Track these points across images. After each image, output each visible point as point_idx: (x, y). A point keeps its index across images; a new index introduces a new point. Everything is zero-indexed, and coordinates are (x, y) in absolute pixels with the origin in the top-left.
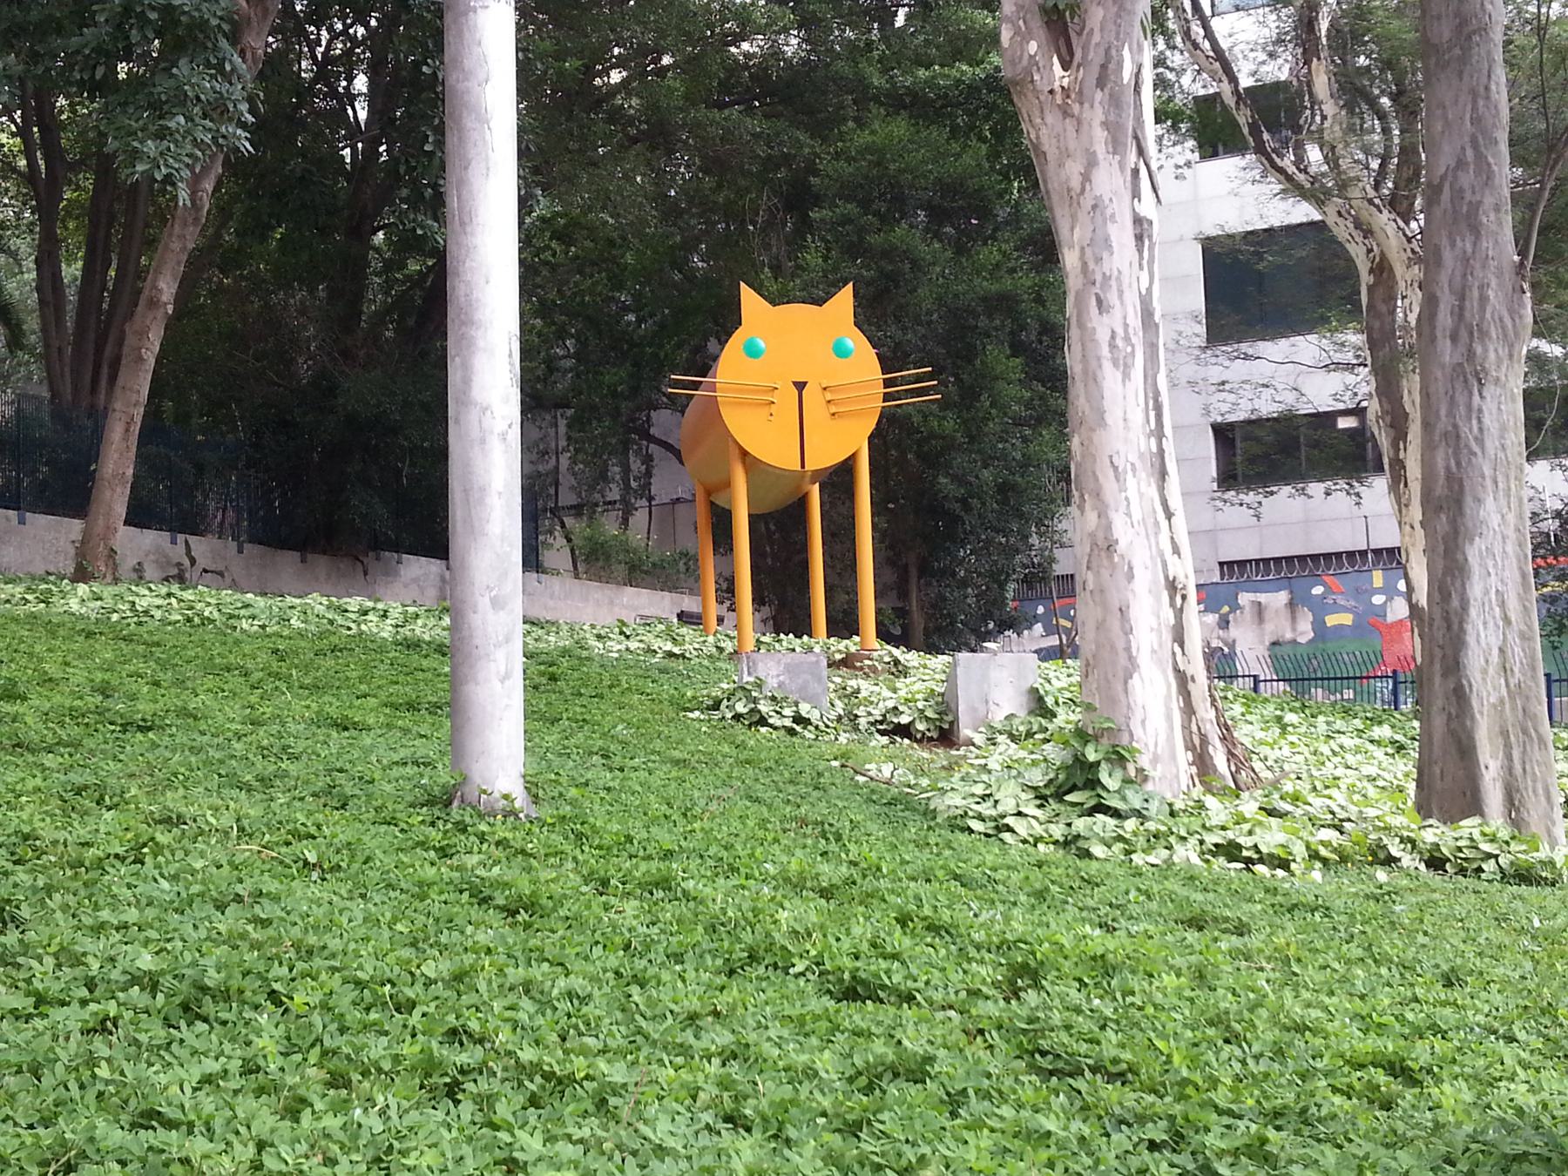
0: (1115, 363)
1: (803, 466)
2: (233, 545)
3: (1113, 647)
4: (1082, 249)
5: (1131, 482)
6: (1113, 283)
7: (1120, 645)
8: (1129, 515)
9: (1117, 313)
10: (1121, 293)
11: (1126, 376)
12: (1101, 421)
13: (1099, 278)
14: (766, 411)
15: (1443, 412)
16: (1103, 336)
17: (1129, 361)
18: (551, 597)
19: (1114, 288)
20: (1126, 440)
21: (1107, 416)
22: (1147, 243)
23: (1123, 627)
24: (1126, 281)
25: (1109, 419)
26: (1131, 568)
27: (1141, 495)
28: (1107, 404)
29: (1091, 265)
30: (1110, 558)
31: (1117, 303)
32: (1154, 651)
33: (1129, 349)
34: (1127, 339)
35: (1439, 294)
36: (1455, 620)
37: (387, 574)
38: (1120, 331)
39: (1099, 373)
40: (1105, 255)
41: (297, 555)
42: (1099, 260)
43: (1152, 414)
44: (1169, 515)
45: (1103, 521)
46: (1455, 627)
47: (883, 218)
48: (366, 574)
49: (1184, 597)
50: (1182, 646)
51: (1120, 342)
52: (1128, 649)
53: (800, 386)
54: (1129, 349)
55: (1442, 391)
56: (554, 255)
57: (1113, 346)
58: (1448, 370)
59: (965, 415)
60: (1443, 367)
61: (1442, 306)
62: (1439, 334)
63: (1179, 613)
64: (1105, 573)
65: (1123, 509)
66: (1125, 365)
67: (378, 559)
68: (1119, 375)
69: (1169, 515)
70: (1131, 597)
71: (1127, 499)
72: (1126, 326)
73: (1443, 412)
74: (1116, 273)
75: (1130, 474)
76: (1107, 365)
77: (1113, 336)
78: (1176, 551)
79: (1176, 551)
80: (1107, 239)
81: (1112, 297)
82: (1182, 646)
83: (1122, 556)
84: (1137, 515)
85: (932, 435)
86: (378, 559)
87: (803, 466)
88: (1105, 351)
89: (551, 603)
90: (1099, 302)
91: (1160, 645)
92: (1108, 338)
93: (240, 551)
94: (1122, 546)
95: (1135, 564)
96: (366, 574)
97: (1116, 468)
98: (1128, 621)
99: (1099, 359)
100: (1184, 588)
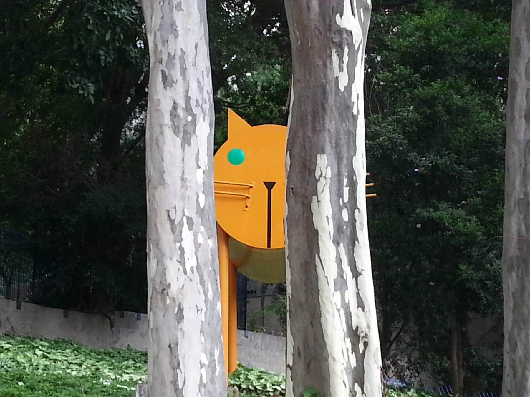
0: (176, 129)
1: (269, 246)
2: (13, 304)
3: (163, 382)
4: (155, 33)
5: (187, 234)
6: (177, 62)
7: (169, 377)
8: (182, 262)
9: (180, 87)
10: (184, 70)
11: (186, 141)
12: (162, 182)
13: (165, 57)
14: (243, 203)
15: (518, 183)
16: (166, 106)
17: (190, 129)
18: (255, 347)
19: (178, 65)
20: (183, 197)
21: (166, 176)
22: (346, 50)
23: (171, 363)
24: (189, 61)
25: (168, 179)
26: (181, 310)
27: (197, 246)
28: (166, 165)
29: (160, 46)
30: (164, 300)
31: (180, 79)
32: (202, 385)
33: (190, 118)
34: (188, 109)
35: (517, 80)
36: (519, 369)
37: (128, 327)
38: (181, 103)
39: (160, 138)
40: (171, 38)
41: (60, 312)
42: (165, 42)
43: (346, 191)
44: (356, 274)
45: (160, 268)
46: (519, 374)
47: (424, 76)
48: (112, 326)
49: (366, 344)
50: (362, 386)
51: (180, 112)
52: (175, 382)
53: (270, 186)
54: (190, 118)
55: (517, 164)
56: (271, 112)
57: (174, 114)
58: (522, 146)
59: (488, 219)
60: (519, 142)
61: (519, 90)
62: (516, 114)
63: (361, 358)
64: (160, 314)
65: (176, 257)
66: (185, 132)
67: (122, 316)
68: (179, 141)
69: (356, 274)
70: (180, 335)
71: (181, 249)
72: (188, 99)
73: (518, 183)
74: (179, 53)
75: (186, 227)
76: (168, 132)
77: (175, 106)
78: (361, 304)
79: (361, 304)
80: (173, 24)
81: (176, 74)
82: (362, 386)
83: (173, 300)
84: (191, 262)
85: (458, 233)
86: (122, 316)
87: (269, 246)
88: (167, 120)
89: (254, 352)
90: (165, 78)
91: (212, 380)
92: (170, 108)
93: (19, 307)
94: (174, 290)
95: (186, 306)
96: (112, 326)
97: (172, 222)
98: (176, 357)
99: (161, 126)
100: (366, 336)
